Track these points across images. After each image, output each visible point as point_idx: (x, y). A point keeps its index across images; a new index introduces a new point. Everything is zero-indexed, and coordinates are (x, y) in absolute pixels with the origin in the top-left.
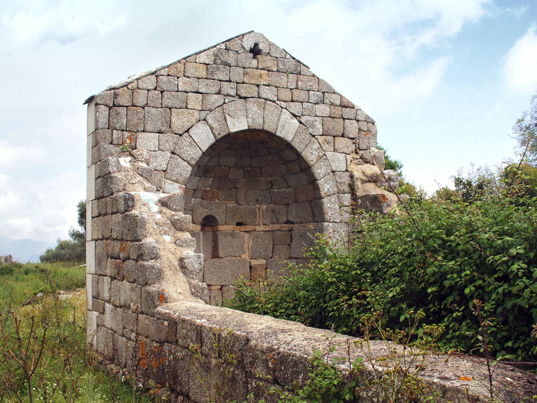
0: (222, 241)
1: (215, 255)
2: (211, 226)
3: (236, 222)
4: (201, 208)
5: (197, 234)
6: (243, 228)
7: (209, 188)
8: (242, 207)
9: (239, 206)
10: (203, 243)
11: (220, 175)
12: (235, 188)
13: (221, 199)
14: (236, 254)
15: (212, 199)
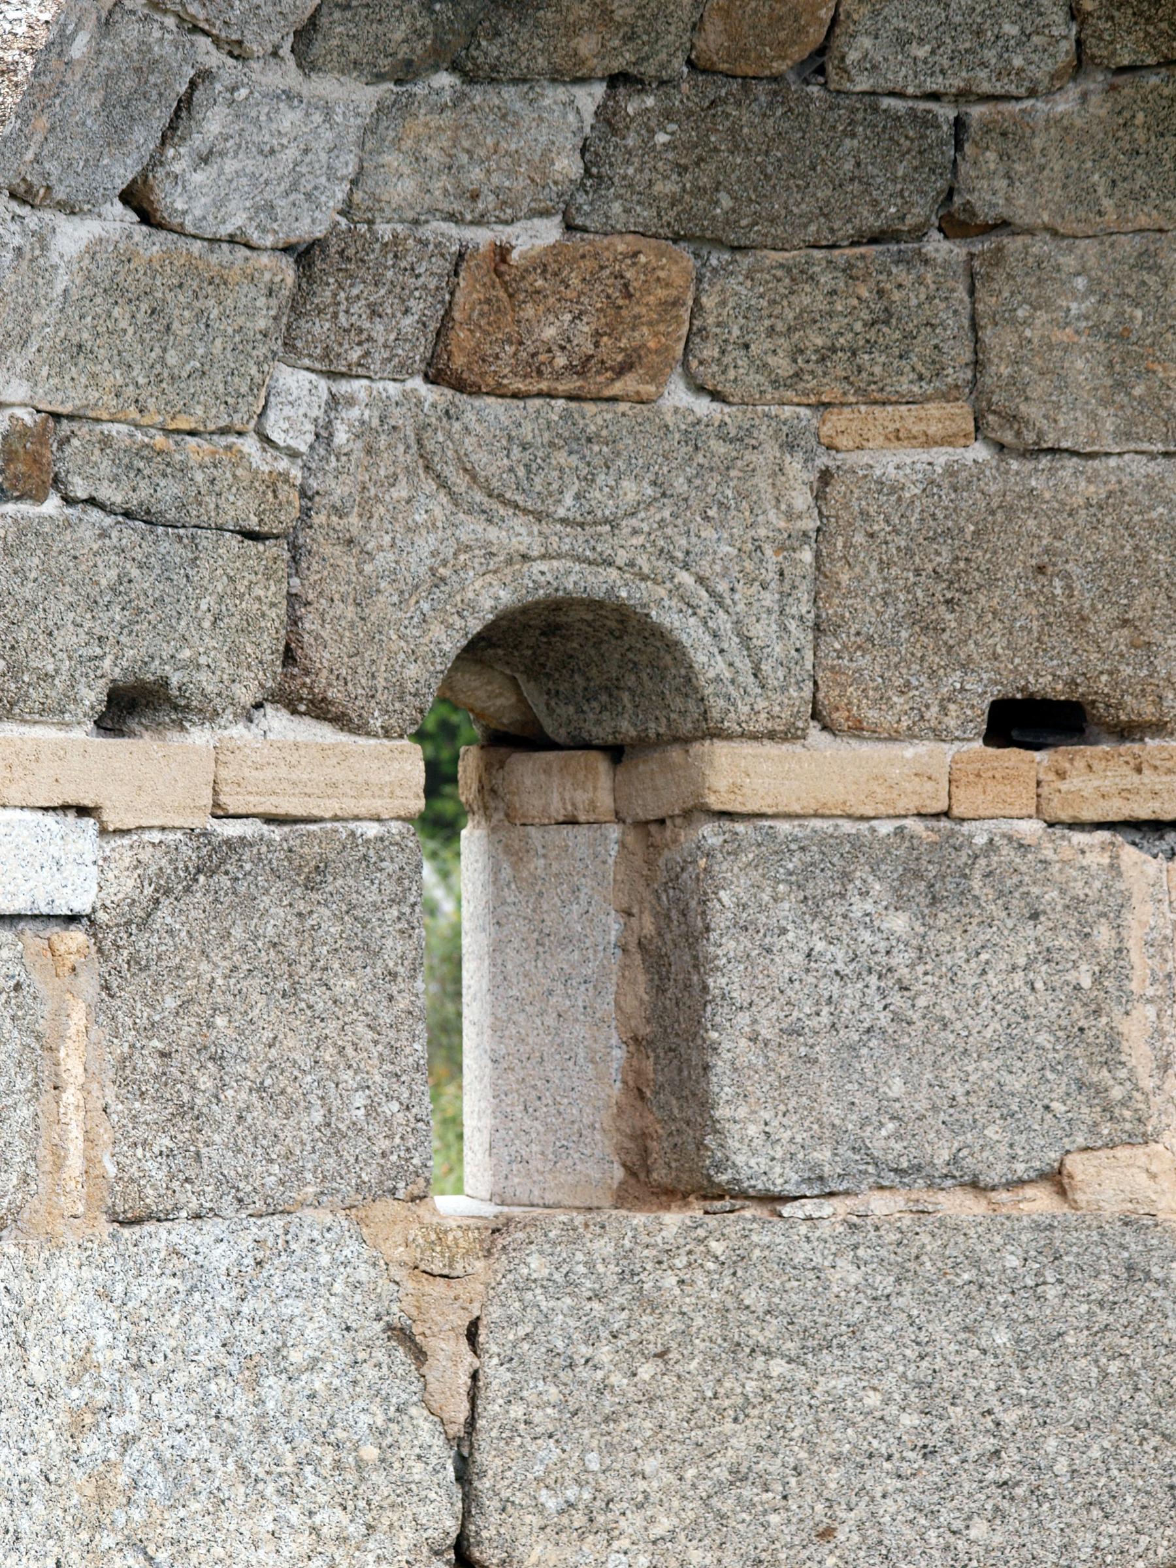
0: (769, 968)
1: (666, 1152)
2: (616, 753)
3: (982, 691)
4: (440, 506)
5: (367, 858)
6: (1092, 778)
7: (549, 232)
8: (1075, 483)
9: (1037, 477)
10: (500, 980)
11: (713, 40)
12: (957, 225)
13: (741, 374)
14: (996, 1147)
15: (590, 377)
